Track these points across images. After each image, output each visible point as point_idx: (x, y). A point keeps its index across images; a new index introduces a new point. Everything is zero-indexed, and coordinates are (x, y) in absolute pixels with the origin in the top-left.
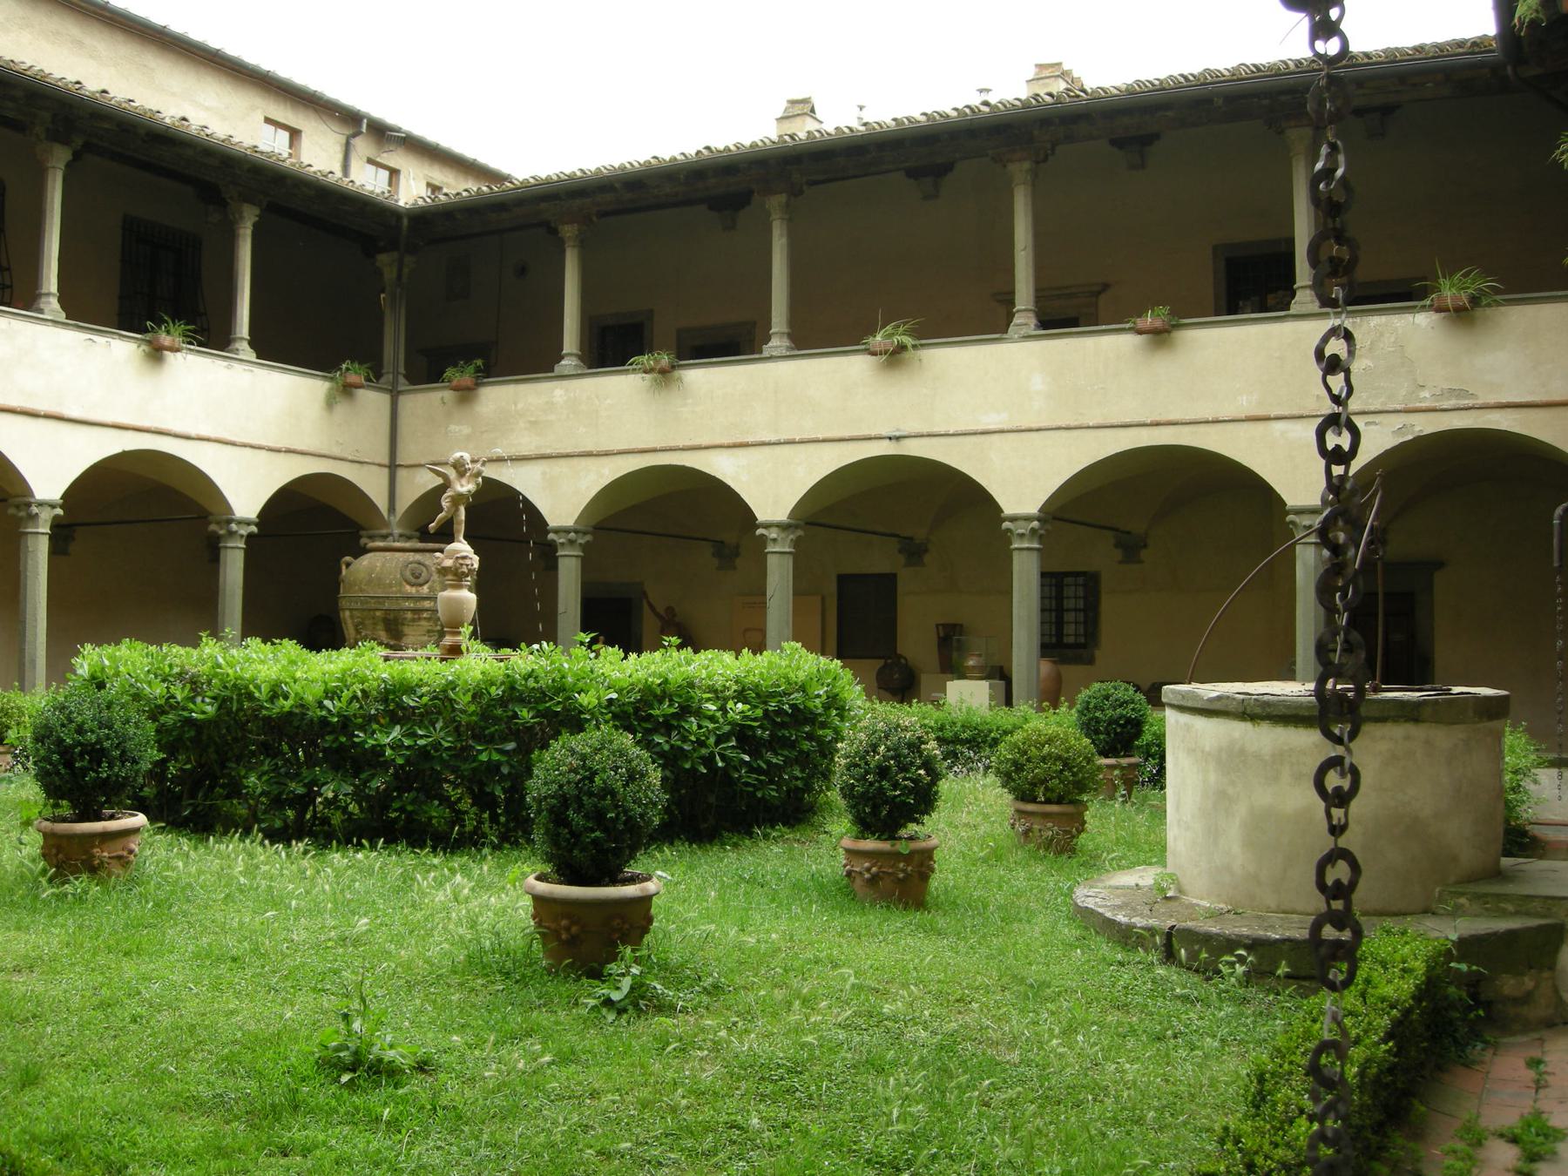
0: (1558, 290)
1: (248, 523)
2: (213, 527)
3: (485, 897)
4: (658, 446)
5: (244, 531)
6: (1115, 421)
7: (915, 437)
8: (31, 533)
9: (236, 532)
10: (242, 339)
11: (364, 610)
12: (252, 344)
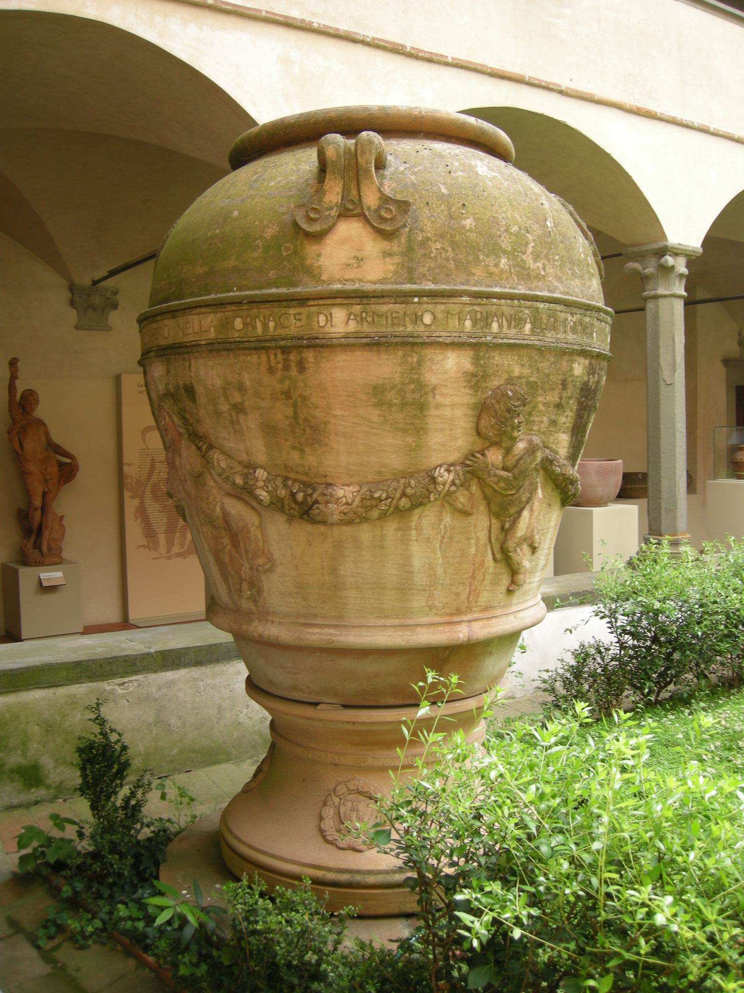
8: (665, 296)
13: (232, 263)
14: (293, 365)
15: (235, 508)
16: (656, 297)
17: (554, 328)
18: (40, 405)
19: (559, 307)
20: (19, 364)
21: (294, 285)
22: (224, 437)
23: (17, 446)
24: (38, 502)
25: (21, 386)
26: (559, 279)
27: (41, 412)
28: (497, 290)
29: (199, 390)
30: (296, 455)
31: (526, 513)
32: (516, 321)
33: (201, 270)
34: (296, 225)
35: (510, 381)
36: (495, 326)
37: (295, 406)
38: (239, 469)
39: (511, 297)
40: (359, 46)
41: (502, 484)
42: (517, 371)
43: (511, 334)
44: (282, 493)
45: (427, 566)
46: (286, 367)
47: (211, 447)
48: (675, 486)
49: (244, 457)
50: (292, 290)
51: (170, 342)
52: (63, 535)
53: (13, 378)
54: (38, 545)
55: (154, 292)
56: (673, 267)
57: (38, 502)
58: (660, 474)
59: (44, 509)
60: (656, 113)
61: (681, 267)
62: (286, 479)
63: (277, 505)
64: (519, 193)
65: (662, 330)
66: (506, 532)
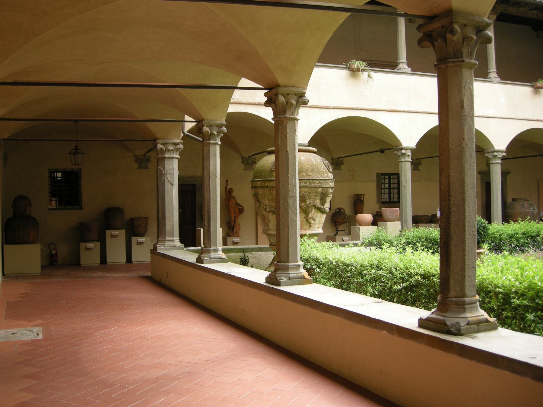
0: (519, 82)
1: (502, 152)
2: (487, 155)
3: (452, 224)
4: (355, 107)
5: (500, 155)
6: (525, 118)
7: (400, 112)
8: (403, 161)
9: (405, 153)
10: (403, 62)
11: (311, 187)
12: (409, 65)
13: (263, 174)
14: (271, 190)
15: (264, 212)
16: (401, 162)
17: (313, 183)
18: (234, 192)
19: (314, 180)
20: (228, 182)
21: (272, 178)
22: (262, 201)
23: (227, 204)
24: (233, 219)
25: (229, 187)
26: (315, 175)
27: (234, 194)
28: (302, 178)
29: (259, 193)
30: (272, 204)
31: (310, 213)
32: (306, 183)
33: (259, 175)
34: (272, 169)
35: (305, 192)
36: (302, 184)
37: (272, 196)
38: (264, 206)
39: (305, 179)
40: (307, 108)
41: (305, 208)
42: (306, 191)
43: (305, 185)
44: (271, 209)
45: (517, 295)
46: (271, 190)
47: (261, 202)
48: (407, 215)
49: (265, 204)
50: (271, 179)
51: (255, 186)
52: (240, 229)
53: (227, 185)
54: (233, 232)
55: (253, 177)
56: (405, 153)
57: (233, 219)
58: (402, 212)
59: (235, 221)
60: (398, 110)
61: (409, 153)
62: (271, 207)
63: (270, 211)
64: (309, 162)
65: (403, 171)
66: (307, 216)
